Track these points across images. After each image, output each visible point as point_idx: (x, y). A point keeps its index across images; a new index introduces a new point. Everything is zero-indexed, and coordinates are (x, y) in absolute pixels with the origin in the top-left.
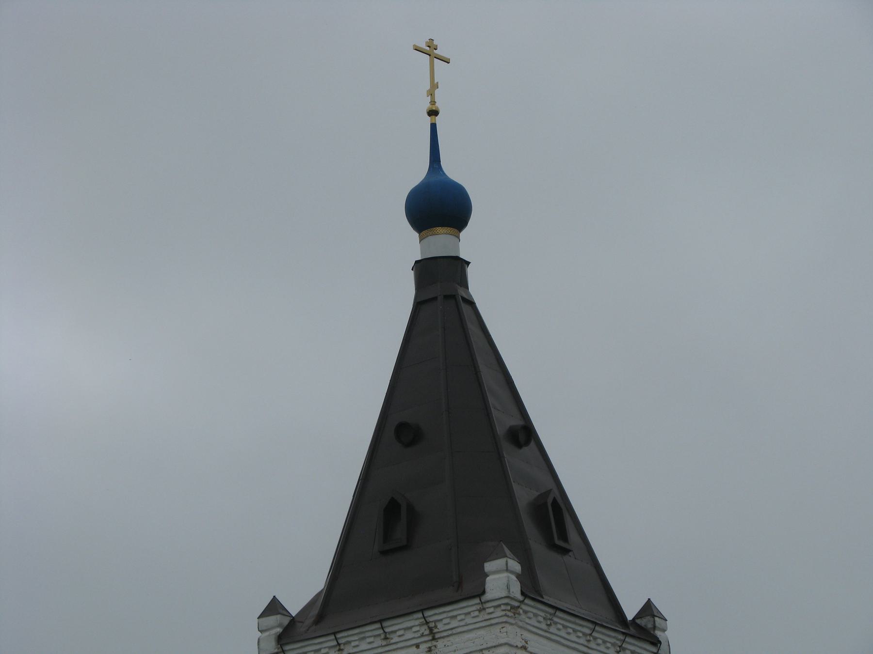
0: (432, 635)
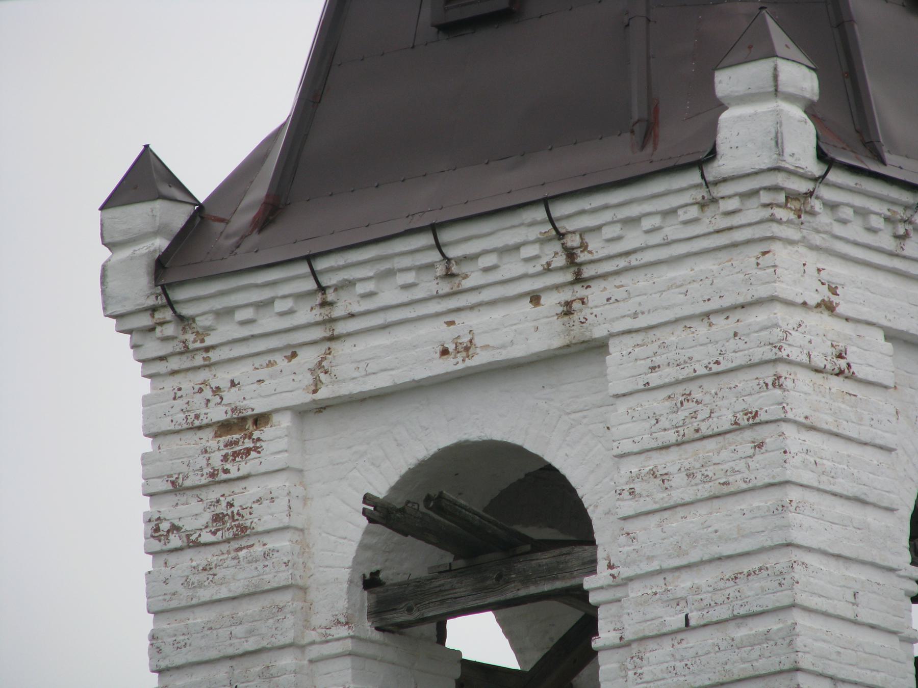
0: (575, 269)
